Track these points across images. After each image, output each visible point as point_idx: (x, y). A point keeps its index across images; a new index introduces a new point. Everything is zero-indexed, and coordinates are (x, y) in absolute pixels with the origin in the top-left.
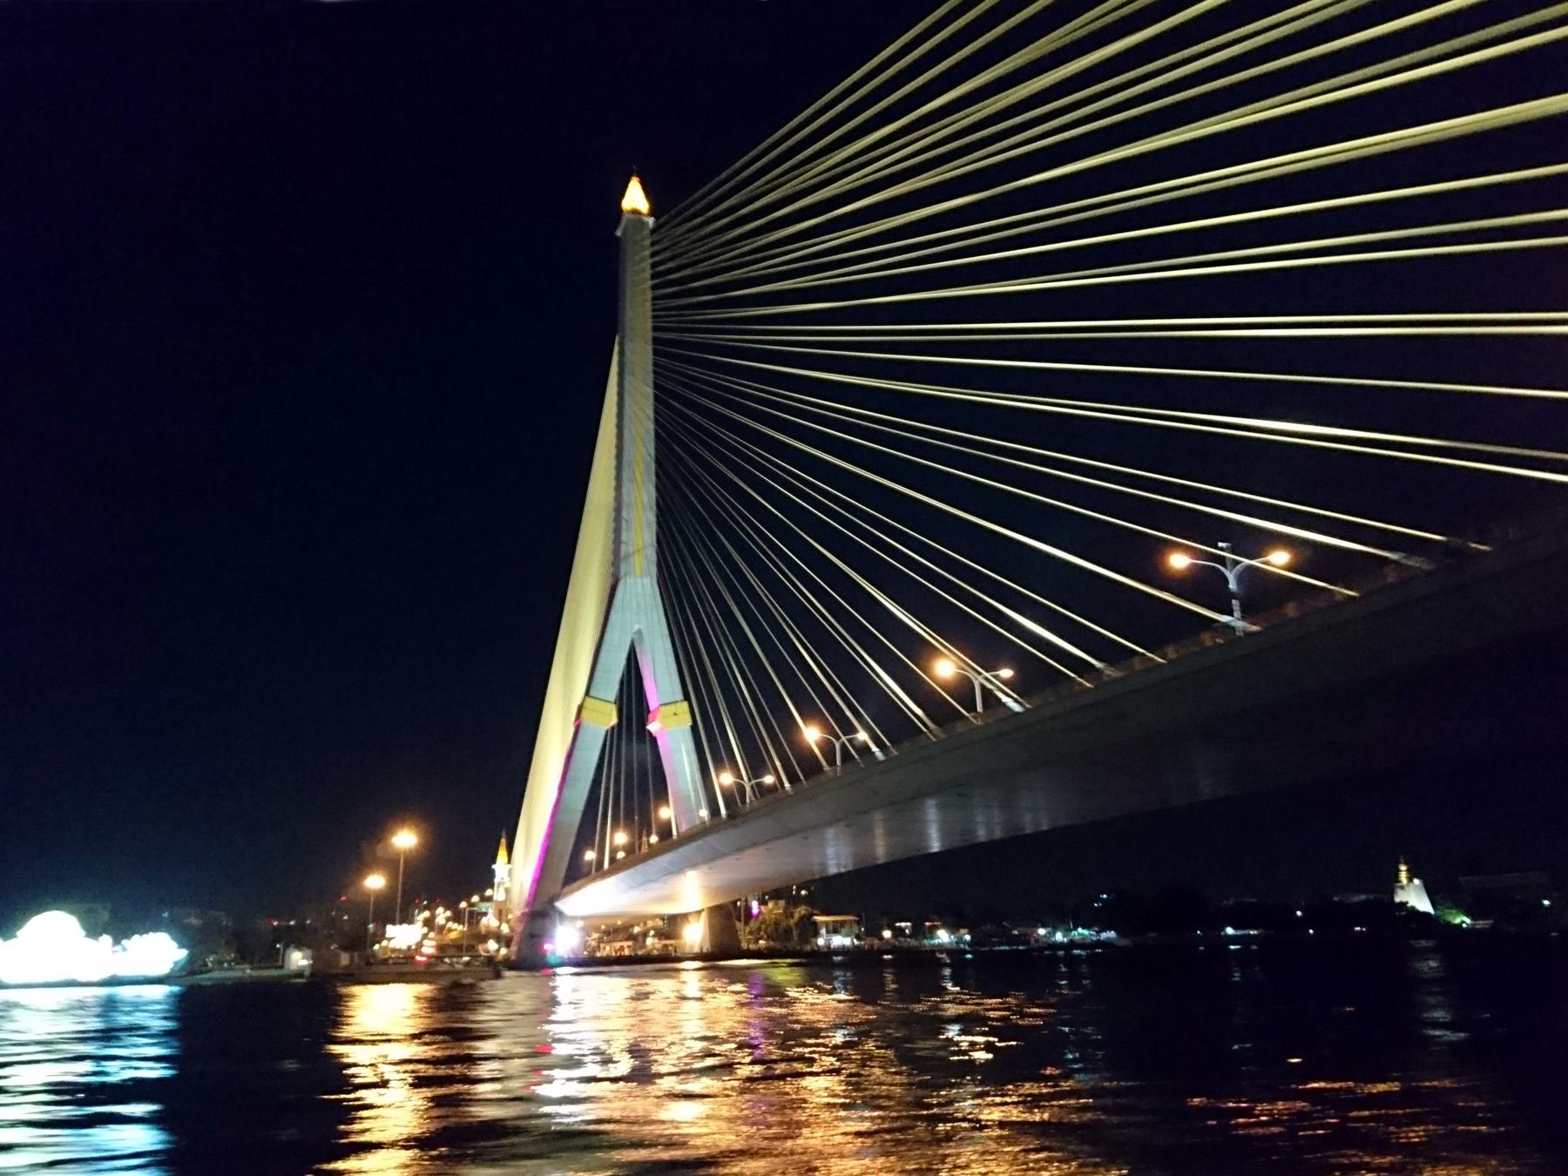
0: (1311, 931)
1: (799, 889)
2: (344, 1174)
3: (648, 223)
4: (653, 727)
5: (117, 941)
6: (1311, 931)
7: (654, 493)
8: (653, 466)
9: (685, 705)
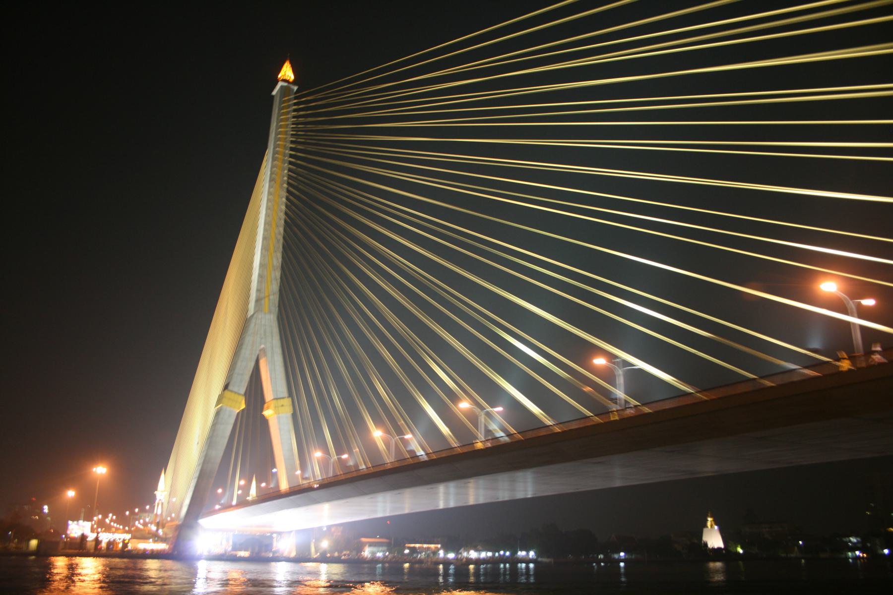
0: (801, 542)
1: (340, 552)
2: (87, 594)
3: (293, 90)
4: (267, 413)
5: (203, 553)
6: (801, 542)
7: (280, 260)
8: (281, 241)
9: (290, 399)
